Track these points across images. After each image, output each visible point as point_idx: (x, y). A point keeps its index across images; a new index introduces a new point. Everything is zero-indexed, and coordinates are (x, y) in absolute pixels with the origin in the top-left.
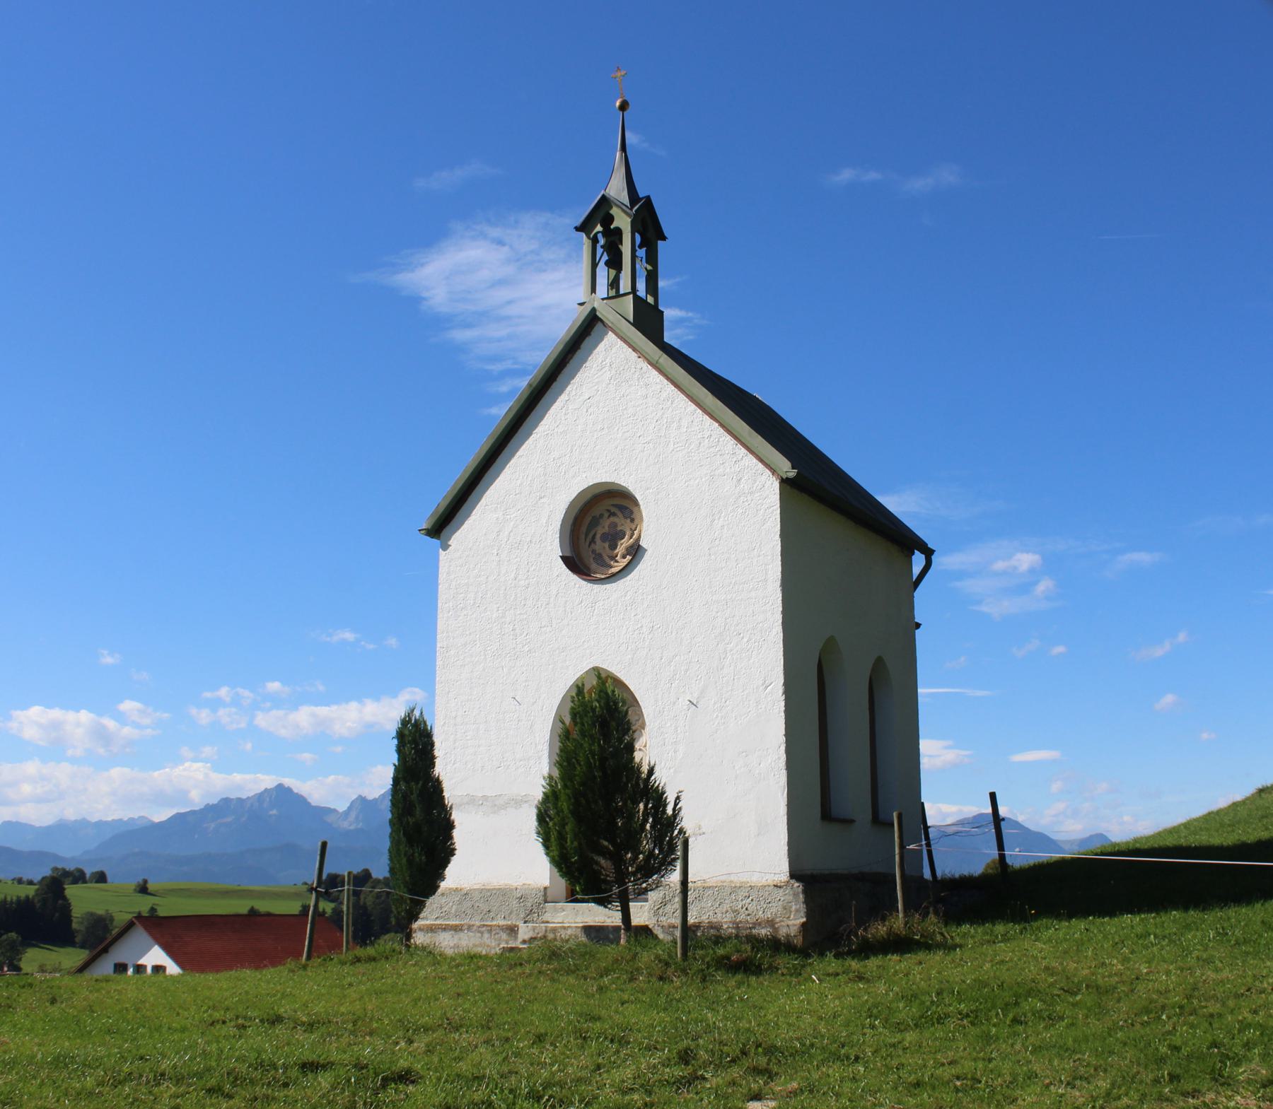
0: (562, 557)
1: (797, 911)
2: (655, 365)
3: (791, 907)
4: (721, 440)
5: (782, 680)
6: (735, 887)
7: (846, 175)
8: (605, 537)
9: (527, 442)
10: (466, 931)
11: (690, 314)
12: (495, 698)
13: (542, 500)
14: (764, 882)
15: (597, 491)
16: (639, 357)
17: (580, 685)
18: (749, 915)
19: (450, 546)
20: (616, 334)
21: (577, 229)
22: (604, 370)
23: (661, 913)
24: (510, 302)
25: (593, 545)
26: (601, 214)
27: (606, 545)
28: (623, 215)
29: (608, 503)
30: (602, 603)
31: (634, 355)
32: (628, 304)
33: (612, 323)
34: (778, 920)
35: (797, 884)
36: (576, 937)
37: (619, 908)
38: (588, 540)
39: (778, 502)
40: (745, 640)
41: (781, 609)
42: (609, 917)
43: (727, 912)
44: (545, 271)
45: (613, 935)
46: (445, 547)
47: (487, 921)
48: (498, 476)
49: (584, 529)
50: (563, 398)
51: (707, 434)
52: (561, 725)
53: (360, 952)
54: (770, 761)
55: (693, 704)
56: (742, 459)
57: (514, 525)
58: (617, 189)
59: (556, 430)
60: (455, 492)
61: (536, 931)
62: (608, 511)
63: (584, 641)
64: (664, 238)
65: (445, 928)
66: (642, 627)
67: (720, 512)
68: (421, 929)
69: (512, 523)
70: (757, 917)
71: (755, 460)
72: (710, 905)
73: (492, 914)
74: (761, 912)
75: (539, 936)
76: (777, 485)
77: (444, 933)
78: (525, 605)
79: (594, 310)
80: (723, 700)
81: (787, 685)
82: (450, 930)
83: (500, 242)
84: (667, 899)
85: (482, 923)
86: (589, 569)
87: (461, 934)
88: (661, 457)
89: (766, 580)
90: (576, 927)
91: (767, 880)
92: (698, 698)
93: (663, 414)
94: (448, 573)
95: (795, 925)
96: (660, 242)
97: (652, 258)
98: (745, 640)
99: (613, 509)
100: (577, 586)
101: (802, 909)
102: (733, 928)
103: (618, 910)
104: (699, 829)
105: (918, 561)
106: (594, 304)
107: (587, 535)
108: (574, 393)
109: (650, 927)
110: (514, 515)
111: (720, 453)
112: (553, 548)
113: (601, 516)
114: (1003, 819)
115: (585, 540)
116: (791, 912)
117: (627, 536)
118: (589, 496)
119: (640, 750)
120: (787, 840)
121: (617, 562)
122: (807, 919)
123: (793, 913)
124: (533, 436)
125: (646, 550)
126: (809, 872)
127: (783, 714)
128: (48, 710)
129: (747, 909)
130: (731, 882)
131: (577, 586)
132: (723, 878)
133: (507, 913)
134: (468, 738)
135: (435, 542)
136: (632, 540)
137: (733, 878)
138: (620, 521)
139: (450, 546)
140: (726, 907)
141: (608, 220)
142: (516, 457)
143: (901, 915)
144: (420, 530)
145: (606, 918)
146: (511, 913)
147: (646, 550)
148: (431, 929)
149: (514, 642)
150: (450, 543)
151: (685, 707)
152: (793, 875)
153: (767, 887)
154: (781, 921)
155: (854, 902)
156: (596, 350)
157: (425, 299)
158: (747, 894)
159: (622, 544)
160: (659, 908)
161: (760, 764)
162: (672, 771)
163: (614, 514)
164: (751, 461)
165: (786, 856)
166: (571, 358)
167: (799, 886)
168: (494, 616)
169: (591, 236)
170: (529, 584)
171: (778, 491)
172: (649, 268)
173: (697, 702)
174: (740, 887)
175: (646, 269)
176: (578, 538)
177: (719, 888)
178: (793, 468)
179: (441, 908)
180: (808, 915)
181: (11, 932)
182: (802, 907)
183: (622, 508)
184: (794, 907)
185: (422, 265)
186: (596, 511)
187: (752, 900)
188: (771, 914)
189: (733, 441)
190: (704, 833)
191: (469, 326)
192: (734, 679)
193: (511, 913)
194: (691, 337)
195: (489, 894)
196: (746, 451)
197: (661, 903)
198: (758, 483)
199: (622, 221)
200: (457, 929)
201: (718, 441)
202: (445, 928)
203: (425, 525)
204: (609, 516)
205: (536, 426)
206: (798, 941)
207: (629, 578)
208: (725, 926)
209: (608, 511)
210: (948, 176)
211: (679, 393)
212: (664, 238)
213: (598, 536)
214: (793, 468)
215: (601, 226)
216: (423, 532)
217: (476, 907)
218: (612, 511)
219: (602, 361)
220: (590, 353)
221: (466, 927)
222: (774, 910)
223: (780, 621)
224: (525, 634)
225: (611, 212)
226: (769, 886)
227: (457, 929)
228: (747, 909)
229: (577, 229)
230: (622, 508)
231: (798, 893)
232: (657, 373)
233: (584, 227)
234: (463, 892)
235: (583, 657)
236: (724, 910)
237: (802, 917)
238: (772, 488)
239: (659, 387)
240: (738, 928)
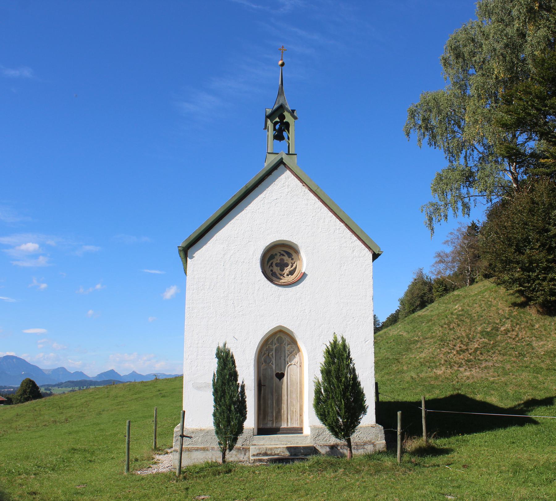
1: (381, 437)
9: (241, 213)
10: (211, 451)
12: (222, 336)
13: (250, 243)
16: (304, 186)
19: (194, 257)
22: (284, 188)
23: (317, 439)
26: (279, 113)
29: (279, 249)
30: (284, 296)
36: (283, 452)
40: (356, 320)
45: (303, 451)
48: (224, 227)
49: (267, 259)
54: (367, 373)
57: (234, 252)
59: (258, 211)
61: (261, 450)
62: (280, 253)
66: (305, 309)
69: (232, 252)
74: (365, 438)
75: (262, 452)
77: (196, 452)
79: (282, 159)
82: (201, 450)
87: (208, 452)
88: (315, 233)
90: (283, 447)
94: (193, 271)
95: (383, 443)
98: (356, 320)
106: (282, 156)
107: (268, 262)
108: (268, 195)
112: (307, 278)
113: (276, 254)
115: (267, 265)
116: (378, 437)
119: (294, 364)
120: (375, 407)
121: (284, 277)
124: (244, 211)
125: (307, 275)
128: (455, 392)
136: (292, 268)
138: (286, 258)
139: (194, 257)
147: (307, 275)
149: (234, 309)
150: (194, 255)
156: (280, 177)
159: (287, 269)
163: (283, 255)
165: (375, 414)
166: (267, 178)
169: (273, 122)
183: (289, 255)
184: (380, 435)
200: (204, 449)
206: (385, 449)
207: (298, 286)
209: (280, 253)
215: (279, 118)
217: (213, 439)
218: (282, 253)
219: (284, 183)
222: (371, 437)
224: (240, 306)
225: (284, 113)
226: (369, 427)
227: (204, 449)
230: (289, 255)
231: (382, 430)
233: (270, 117)
235: (273, 320)
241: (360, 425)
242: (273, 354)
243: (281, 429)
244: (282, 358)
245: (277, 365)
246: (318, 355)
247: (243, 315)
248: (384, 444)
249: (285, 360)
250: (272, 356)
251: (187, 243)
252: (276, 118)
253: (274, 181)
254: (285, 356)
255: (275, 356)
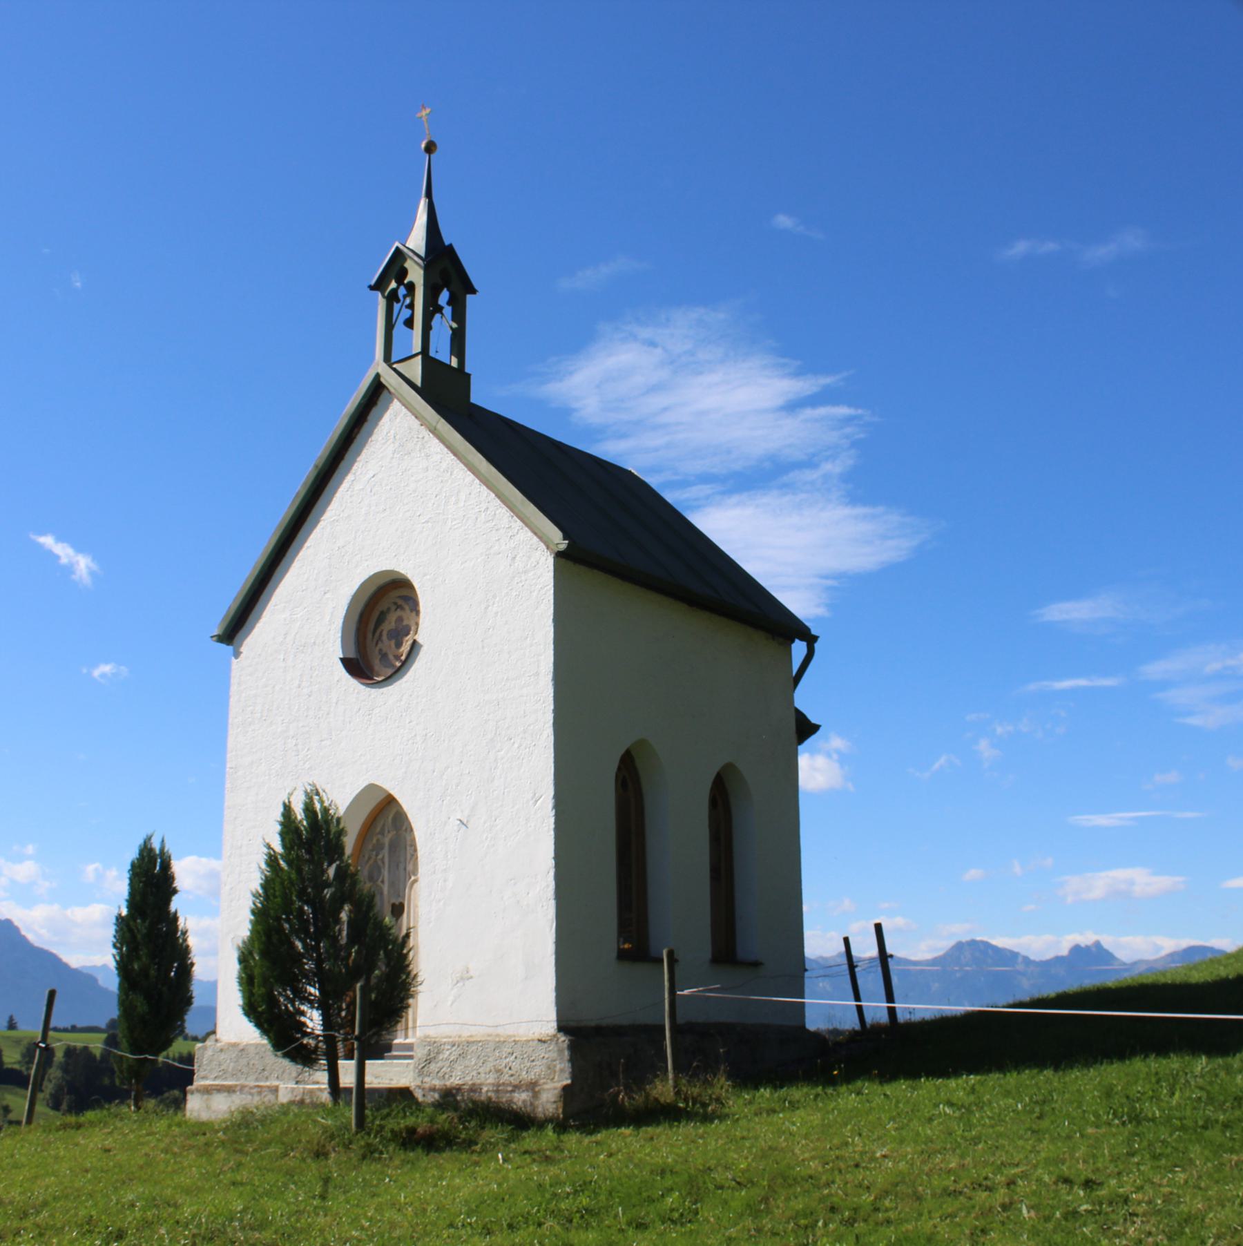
0: (343, 660)
1: (562, 1071)
2: (434, 431)
3: (555, 1066)
4: (497, 512)
5: (551, 792)
6: (499, 1041)
7: (1021, 247)
8: (390, 637)
10: (238, 1093)
11: (860, 411)
13: (327, 596)
14: (531, 1036)
15: (382, 581)
17: (287, 801)
18: (512, 1075)
20: (400, 401)
21: (372, 288)
24: (665, 409)
25: (380, 645)
26: (396, 269)
27: (393, 643)
28: (417, 267)
31: (417, 423)
32: (415, 370)
33: (395, 389)
34: (542, 1081)
35: (563, 1038)
37: (326, 1068)
38: (375, 641)
39: (552, 580)
40: (516, 745)
41: (552, 707)
42: (376, 1077)
43: (490, 1071)
44: (701, 373)
46: (237, 654)
47: (261, 1081)
49: (371, 626)
50: (349, 478)
51: (484, 506)
52: (266, 850)
53: (72, 1119)
55: (463, 824)
56: (517, 533)
58: (417, 240)
60: (245, 592)
61: (295, 1094)
62: (395, 603)
63: (361, 755)
64: (473, 291)
65: (220, 1089)
66: (415, 735)
67: (495, 597)
68: (198, 1091)
70: (521, 1078)
71: (530, 534)
72: (473, 1063)
73: (266, 1073)
74: (524, 1073)
76: (551, 561)
78: (307, 716)
80: (493, 819)
81: (557, 797)
82: (225, 1091)
83: (652, 344)
84: (432, 1055)
85: (257, 1084)
86: (371, 669)
89: (537, 674)
91: (534, 1034)
92: (469, 816)
93: (443, 487)
96: (469, 297)
97: (459, 315)
98: (516, 745)
99: (400, 602)
100: (356, 691)
101: (566, 1069)
102: (493, 1091)
103: (324, 1070)
104: (468, 972)
105: (799, 649)
109: (412, 1089)
110: (301, 614)
111: (496, 527)
112: (334, 649)
113: (389, 609)
114: (891, 956)
116: (555, 1072)
117: (411, 632)
118: (373, 589)
122: (572, 1081)
123: (557, 1074)
126: (593, 1024)
127: (552, 833)
129: (510, 1068)
130: (498, 1035)
131: (356, 691)
132: (490, 1030)
133: (280, 1072)
134: (252, 870)
135: (227, 649)
137: (500, 1031)
140: (489, 1065)
141: (404, 272)
142: (304, 549)
143: (671, 1075)
144: (212, 637)
145: (373, 1079)
146: (283, 1072)
148: (207, 1091)
151: (456, 828)
152: (561, 1028)
153: (531, 1043)
154: (544, 1083)
155: (622, 1060)
157: (574, 410)
158: (510, 1050)
159: (407, 641)
160: (423, 1067)
161: (528, 893)
162: (442, 903)
163: (402, 608)
164: (526, 534)
166: (358, 432)
167: (564, 1041)
168: (279, 730)
169: (386, 294)
170: (311, 692)
171: (552, 568)
172: (455, 325)
173: (467, 822)
174: (504, 1042)
175: (451, 328)
176: (365, 638)
177: (483, 1043)
178: (564, 539)
179: (220, 1065)
180: (574, 1076)
181: (173, 1088)
182: (567, 1066)
185: (571, 374)
186: (383, 606)
187: (516, 1058)
188: (535, 1075)
189: (509, 513)
190: (471, 977)
191: (623, 436)
192: (504, 793)
193: (283, 1072)
194: (862, 436)
195: (263, 1049)
196: (521, 524)
197: (426, 1061)
198: (532, 559)
199: (416, 274)
201: (495, 514)
202: (220, 1089)
203: (216, 631)
204: (396, 610)
205: (323, 512)
208: (485, 1089)
210: (1132, 241)
211: (458, 462)
212: (473, 291)
213: (385, 633)
214: (564, 539)
215: (396, 282)
216: (215, 639)
217: (251, 1066)
220: (376, 424)
221: (238, 1088)
222: (537, 1070)
223: (552, 722)
227: (230, 1090)
228: (510, 1068)
229: (372, 288)
232: (437, 441)
233: (379, 286)
234: (241, 1047)
236: (488, 1070)
237: (567, 1079)
238: (547, 563)
239: (439, 456)
240: (497, 1091)
241: (193, 1006)
242: (383, 857)
243: (394, 1047)
244: (401, 866)
245: (392, 884)
246: (439, 849)
247: (310, 768)
248: (556, 1092)
249: (405, 869)
250: (383, 863)
251: (224, 626)
252: (390, 283)
253: (370, 434)
254: (406, 859)
255: (390, 861)
